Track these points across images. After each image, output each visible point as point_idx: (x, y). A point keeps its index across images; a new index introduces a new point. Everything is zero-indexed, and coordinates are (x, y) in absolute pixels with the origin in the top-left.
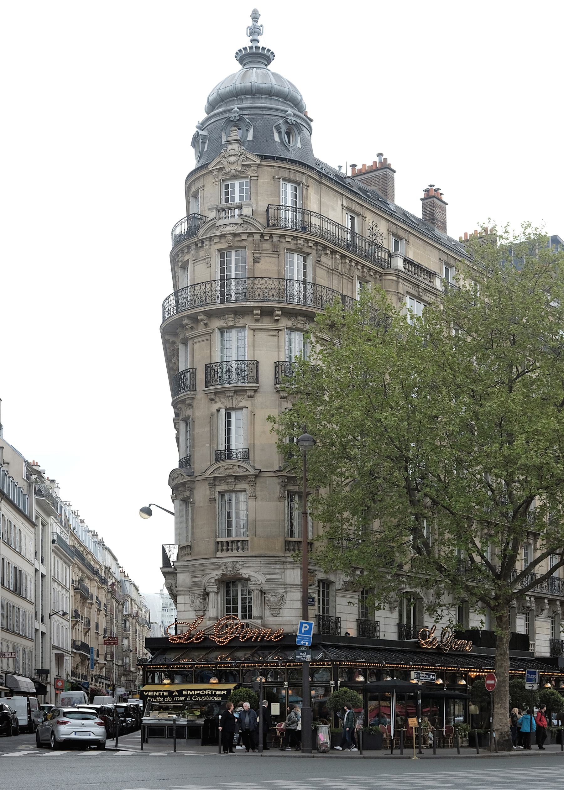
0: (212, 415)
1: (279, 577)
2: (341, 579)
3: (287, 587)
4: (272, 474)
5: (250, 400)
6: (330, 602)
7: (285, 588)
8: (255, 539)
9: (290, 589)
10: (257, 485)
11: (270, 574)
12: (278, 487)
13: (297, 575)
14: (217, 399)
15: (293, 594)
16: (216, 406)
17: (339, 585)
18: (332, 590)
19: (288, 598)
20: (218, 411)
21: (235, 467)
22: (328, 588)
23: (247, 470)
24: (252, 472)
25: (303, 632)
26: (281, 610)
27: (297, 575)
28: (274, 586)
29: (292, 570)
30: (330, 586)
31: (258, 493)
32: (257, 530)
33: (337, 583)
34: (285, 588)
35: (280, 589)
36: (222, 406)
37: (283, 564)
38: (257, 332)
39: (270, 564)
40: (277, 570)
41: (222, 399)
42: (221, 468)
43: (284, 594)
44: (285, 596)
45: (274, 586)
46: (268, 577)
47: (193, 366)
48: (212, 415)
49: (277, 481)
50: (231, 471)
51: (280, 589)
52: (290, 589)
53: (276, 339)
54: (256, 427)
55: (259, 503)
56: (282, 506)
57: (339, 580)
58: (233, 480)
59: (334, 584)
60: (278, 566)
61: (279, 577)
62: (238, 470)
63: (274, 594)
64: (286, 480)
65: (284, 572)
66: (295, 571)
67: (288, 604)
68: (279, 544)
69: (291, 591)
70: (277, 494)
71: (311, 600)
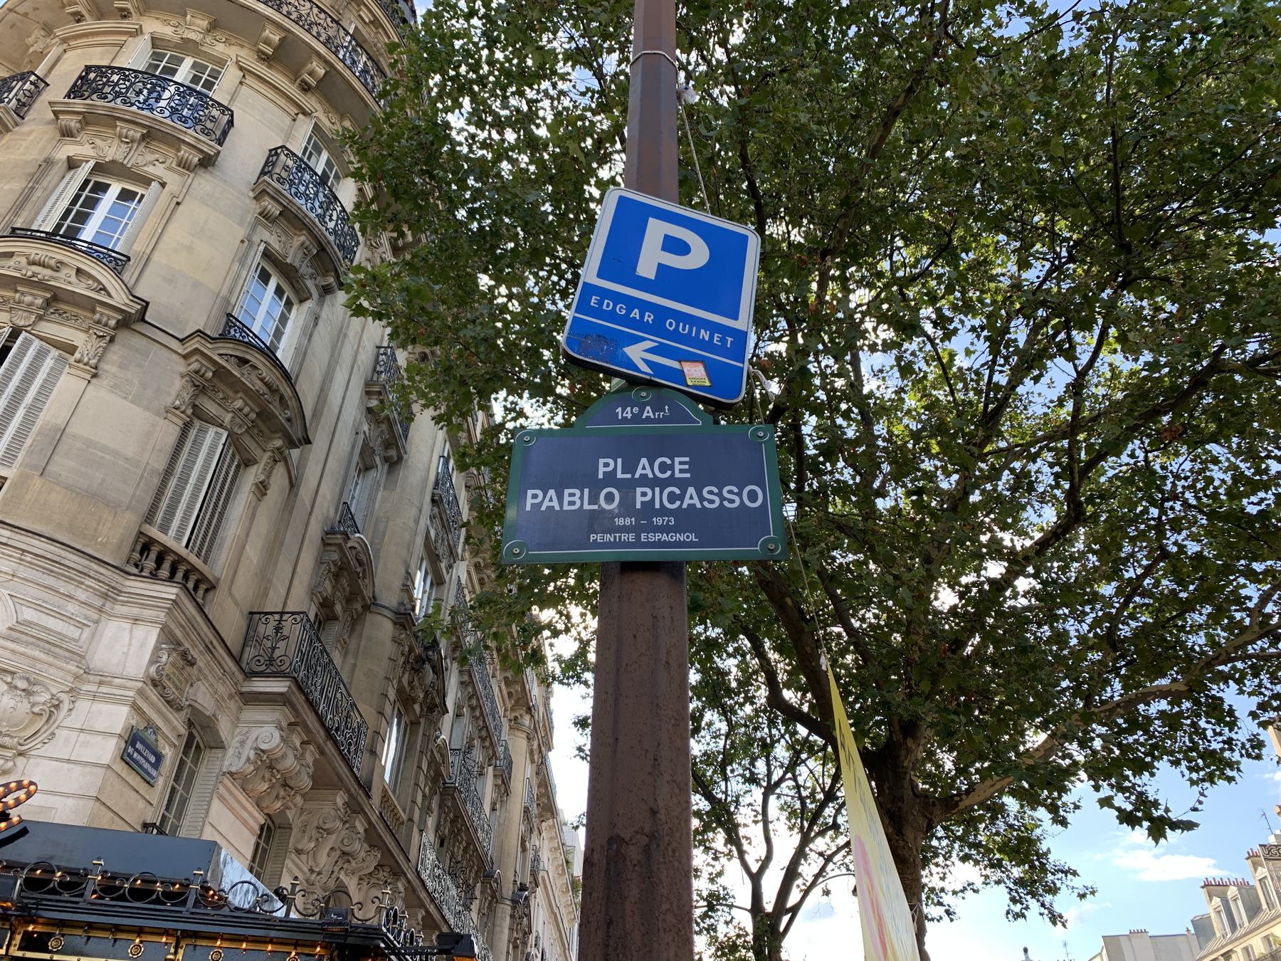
0: (49, 162)
1: (73, 632)
2: (249, 743)
3: (88, 678)
4: (175, 345)
5: (182, 175)
6: (191, 807)
7: (77, 677)
8: (37, 482)
9: (93, 688)
10: (115, 347)
11: (38, 607)
12: (178, 383)
13: (143, 645)
14: (83, 137)
15: (97, 706)
16: (69, 150)
17: (236, 757)
18: (209, 768)
19: (75, 720)
20: (72, 164)
21: (65, 271)
22: (196, 761)
23: (104, 289)
24: (119, 298)
25: (646, 268)
26: (21, 761)
27: (143, 645)
28: (37, 653)
29: (126, 625)
30: (207, 755)
31: (109, 367)
32: (56, 457)
33: (230, 752)
34: (77, 677)
35: (57, 676)
36: (91, 153)
37: (105, 596)
38: (250, 80)
39: (58, 576)
40: (72, 608)
41: (98, 141)
42: (15, 258)
43: (64, 697)
44: (65, 706)
45: (37, 653)
46: (29, 614)
47: (46, 75)
48: (49, 162)
49: (181, 366)
50: (48, 272)
51: (57, 676)
52: (93, 688)
53: (288, 120)
54: (170, 227)
55: (99, 393)
56: (168, 432)
57: (243, 743)
58: (39, 301)
59: (219, 753)
60: (82, 595)
61: (73, 632)
62: (73, 279)
63: (22, 684)
64: (209, 375)
65: (97, 622)
66: (140, 631)
67: (64, 743)
68: (114, 533)
69: (94, 697)
70: (169, 400)
71: (153, 759)
